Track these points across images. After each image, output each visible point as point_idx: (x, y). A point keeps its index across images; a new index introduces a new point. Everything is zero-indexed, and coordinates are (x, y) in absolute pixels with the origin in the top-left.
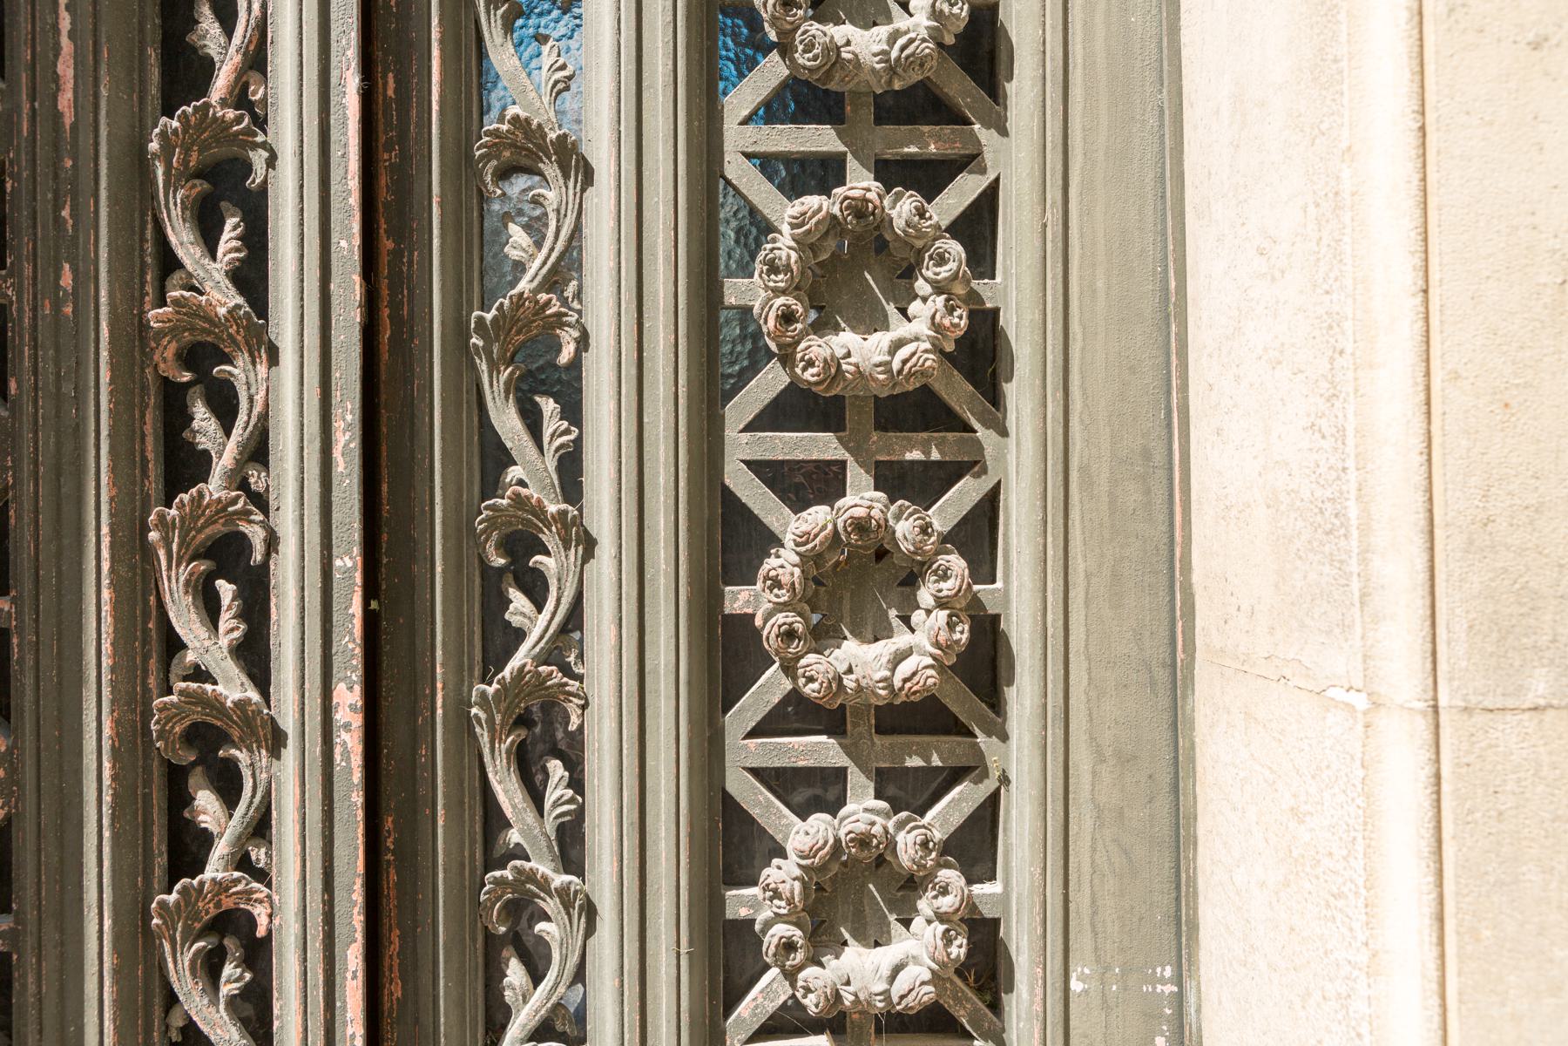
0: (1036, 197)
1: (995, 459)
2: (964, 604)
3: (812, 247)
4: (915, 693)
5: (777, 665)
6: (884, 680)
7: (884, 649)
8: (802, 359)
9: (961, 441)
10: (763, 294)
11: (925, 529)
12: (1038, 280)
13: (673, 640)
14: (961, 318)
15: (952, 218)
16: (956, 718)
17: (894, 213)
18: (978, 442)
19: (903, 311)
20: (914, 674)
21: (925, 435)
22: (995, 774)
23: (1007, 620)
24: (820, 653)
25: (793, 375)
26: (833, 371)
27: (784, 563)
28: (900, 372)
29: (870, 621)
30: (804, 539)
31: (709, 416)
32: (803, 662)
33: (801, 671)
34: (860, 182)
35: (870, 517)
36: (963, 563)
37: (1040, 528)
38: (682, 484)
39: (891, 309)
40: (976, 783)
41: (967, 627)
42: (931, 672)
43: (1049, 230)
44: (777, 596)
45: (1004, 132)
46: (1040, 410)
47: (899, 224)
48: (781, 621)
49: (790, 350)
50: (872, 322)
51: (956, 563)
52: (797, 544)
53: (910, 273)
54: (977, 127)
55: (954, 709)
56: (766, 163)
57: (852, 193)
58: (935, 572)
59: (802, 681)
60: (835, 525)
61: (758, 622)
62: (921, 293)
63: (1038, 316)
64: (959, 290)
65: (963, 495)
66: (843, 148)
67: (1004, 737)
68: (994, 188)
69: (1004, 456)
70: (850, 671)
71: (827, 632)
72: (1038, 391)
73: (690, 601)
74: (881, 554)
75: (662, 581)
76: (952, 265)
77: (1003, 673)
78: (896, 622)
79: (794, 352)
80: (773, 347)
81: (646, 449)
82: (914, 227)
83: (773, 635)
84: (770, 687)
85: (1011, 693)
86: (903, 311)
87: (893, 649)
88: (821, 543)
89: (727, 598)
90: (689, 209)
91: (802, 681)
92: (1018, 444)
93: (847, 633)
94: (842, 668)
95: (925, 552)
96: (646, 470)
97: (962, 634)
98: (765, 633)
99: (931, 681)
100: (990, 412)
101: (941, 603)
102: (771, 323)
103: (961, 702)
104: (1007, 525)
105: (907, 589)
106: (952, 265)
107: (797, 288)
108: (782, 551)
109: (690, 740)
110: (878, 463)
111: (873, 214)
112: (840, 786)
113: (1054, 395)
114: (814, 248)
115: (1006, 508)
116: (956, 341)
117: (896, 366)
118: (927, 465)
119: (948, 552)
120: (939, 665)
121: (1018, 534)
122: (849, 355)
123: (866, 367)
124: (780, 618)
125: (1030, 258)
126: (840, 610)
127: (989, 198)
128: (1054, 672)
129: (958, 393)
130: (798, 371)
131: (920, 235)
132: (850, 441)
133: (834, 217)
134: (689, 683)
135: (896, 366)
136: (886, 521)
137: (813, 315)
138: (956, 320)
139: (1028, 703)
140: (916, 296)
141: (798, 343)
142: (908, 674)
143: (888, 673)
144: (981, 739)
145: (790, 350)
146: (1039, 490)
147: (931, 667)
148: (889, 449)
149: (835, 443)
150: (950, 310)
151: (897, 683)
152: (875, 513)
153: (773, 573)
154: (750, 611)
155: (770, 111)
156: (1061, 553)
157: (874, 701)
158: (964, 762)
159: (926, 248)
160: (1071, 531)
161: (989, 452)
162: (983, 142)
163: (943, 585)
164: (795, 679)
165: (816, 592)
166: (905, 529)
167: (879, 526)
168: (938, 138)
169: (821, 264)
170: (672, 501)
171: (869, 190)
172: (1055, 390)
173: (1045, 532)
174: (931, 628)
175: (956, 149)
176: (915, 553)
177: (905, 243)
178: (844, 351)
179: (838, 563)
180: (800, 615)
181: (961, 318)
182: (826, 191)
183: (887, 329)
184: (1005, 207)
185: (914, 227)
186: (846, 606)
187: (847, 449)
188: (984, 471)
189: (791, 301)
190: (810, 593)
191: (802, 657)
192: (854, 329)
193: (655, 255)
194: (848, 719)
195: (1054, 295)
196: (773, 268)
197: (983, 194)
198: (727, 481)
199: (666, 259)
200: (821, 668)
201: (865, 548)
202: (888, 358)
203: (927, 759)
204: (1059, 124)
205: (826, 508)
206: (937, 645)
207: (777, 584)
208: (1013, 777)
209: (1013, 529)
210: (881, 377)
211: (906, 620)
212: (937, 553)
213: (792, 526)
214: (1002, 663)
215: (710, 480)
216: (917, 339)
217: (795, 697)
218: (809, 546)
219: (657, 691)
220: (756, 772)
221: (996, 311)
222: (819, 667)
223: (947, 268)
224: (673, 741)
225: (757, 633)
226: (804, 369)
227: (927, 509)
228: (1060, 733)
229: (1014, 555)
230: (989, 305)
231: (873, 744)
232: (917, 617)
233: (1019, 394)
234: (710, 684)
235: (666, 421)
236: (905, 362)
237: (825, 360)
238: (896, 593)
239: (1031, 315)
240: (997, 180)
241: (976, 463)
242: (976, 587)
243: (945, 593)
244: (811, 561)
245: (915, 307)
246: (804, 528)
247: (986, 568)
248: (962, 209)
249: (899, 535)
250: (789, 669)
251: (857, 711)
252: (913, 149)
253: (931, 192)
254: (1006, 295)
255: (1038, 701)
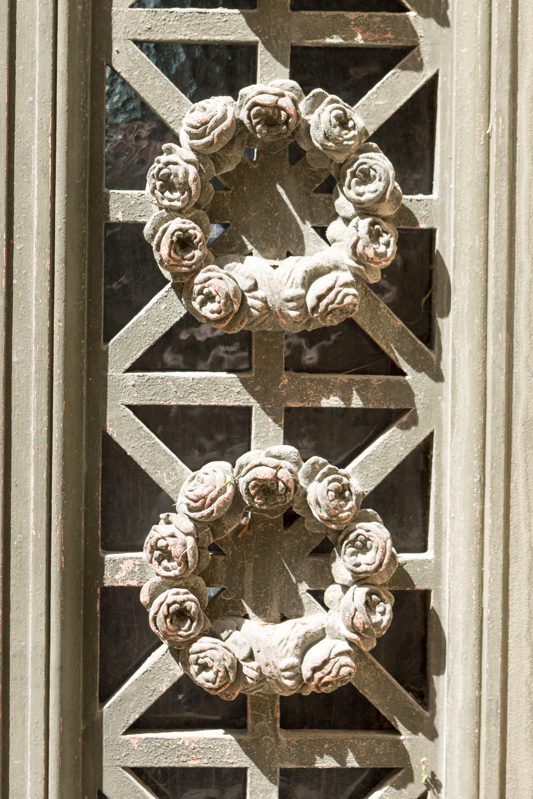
0: (479, 102)
1: (428, 408)
2: (386, 578)
3: (214, 158)
4: (326, 684)
5: (165, 647)
6: (291, 668)
7: (293, 630)
8: (200, 292)
9: (387, 386)
10: (157, 212)
11: (341, 493)
12: (480, 201)
13: (43, 620)
14: (387, 245)
15: (381, 122)
16: (378, 713)
17: (312, 119)
18: (407, 387)
19: (322, 231)
20: (326, 662)
21: (343, 378)
22: (422, 777)
23: (439, 597)
24: (215, 635)
25: (189, 306)
26: (236, 307)
27: (174, 530)
28: (315, 309)
29: (276, 597)
30: (199, 503)
31: (89, 353)
32: (195, 647)
33: (193, 657)
34: (273, 83)
35: (276, 479)
36: (385, 533)
37: (476, 491)
38: (57, 435)
39: (307, 229)
40: (398, 788)
41: (389, 607)
42: (346, 660)
43: (493, 141)
44: (167, 569)
45: (444, 21)
46: (480, 354)
47: (317, 136)
48: (169, 600)
49: (186, 280)
50: (288, 245)
51: (377, 531)
52: (191, 509)
53: (330, 186)
54: (412, 14)
55: (375, 701)
56: (152, 416)
57: (261, 99)
58: (352, 543)
59: (194, 669)
60: (236, 486)
61: (144, 598)
62: (342, 213)
63: (478, 244)
64: (387, 210)
65: (388, 450)
66: (257, 38)
67: (432, 735)
68: (431, 86)
69: (438, 404)
70: (251, 657)
71: (225, 610)
72: (478, 331)
73: (63, 573)
74: (290, 518)
75: (31, 548)
76: (376, 186)
77: (432, 659)
78: (307, 599)
79: (191, 284)
80: (167, 275)
81: (15, 393)
82: (334, 140)
83: (160, 616)
84: (155, 674)
85: (441, 684)
86: (322, 231)
87: (302, 632)
88: (219, 509)
89: (108, 567)
90: (70, 112)
91: (194, 669)
92: (454, 391)
93: (249, 611)
94: (241, 654)
95: (340, 520)
96: (14, 419)
97: (383, 614)
98: (152, 611)
99: (344, 671)
100: (422, 352)
101: (360, 579)
102: (165, 250)
103: (383, 692)
104: (439, 485)
105: (320, 560)
106: (376, 186)
107: (197, 206)
108: (173, 516)
109: (62, 735)
110: (288, 410)
111: (286, 122)
112: (240, 785)
113: (495, 337)
114: (216, 159)
115: (439, 465)
116: (383, 271)
117: (310, 301)
118: (345, 412)
119: (368, 519)
120: (356, 652)
121: (453, 497)
122: (255, 287)
123: (275, 302)
124: (170, 595)
125: (471, 173)
126: (241, 583)
127: (425, 102)
128: (490, 660)
129: (387, 330)
130: (196, 305)
131: (341, 148)
132: (255, 384)
133: (239, 123)
134: (62, 669)
135: (310, 301)
136: (296, 482)
137: (216, 230)
138: (382, 249)
139: (460, 695)
140: (336, 216)
141: (196, 272)
142: (318, 662)
143: (295, 661)
144: (405, 736)
145: (186, 280)
146: (477, 447)
147: (346, 653)
148: (302, 395)
149: (238, 387)
150: (374, 236)
151: (306, 673)
152: (284, 474)
153: (161, 543)
154: (134, 583)
155: (149, 361)
156: (500, 521)
157: (278, 691)
158: (384, 763)
159: (348, 163)
160: (513, 495)
161: (420, 399)
162: (420, 32)
163: (361, 558)
164: (186, 665)
165: (213, 562)
166: (318, 493)
167: (287, 489)
168: (366, 28)
169: (226, 176)
170: (44, 456)
171: (282, 95)
172: (497, 330)
173: (483, 496)
174: (346, 609)
175: (389, 40)
176: (327, 520)
177: (323, 154)
178: (251, 283)
179: (240, 528)
180: (193, 591)
181: (387, 245)
182: (232, 91)
183: (302, 253)
184: (444, 110)
185: (334, 140)
186: (249, 579)
187: (253, 393)
188: (414, 421)
189: (189, 224)
190: (205, 564)
191: (195, 640)
192: (263, 252)
193: (28, 165)
194: (249, 712)
195: (498, 219)
196: (167, 184)
197: (424, 88)
198: (110, 430)
199: (42, 170)
200: (217, 655)
201: (272, 512)
202: (301, 291)
203: (341, 759)
204: (507, 18)
205: (225, 465)
206: (353, 628)
207: (166, 554)
208: (442, 778)
209: (447, 490)
210: (293, 314)
211: (318, 595)
212: (357, 519)
213: (185, 487)
214: (432, 646)
215: (89, 429)
216: (336, 268)
217: (185, 684)
218: (205, 512)
219: (23, 678)
220: (139, 773)
221: (431, 233)
222: (214, 654)
223: (371, 187)
224: (41, 737)
225: (142, 611)
226: (203, 304)
227: (343, 465)
228: (496, 731)
229: (447, 522)
230: (423, 225)
231: (278, 741)
232: (332, 593)
233: (456, 331)
234: (85, 669)
235: (39, 361)
236: (320, 298)
237: (227, 296)
238: (308, 563)
239: (471, 242)
240: (436, 76)
241: (404, 411)
242: (402, 557)
243: (363, 568)
244: (210, 531)
245: (335, 228)
246: (200, 490)
247: (415, 533)
248: (392, 112)
249: (310, 499)
250: (179, 652)
251: (259, 703)
252: (336, 40)
253: (353, 93)
254: (443, 214)
255: (472, 694)
